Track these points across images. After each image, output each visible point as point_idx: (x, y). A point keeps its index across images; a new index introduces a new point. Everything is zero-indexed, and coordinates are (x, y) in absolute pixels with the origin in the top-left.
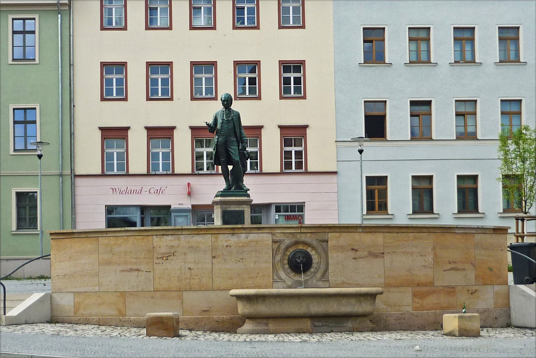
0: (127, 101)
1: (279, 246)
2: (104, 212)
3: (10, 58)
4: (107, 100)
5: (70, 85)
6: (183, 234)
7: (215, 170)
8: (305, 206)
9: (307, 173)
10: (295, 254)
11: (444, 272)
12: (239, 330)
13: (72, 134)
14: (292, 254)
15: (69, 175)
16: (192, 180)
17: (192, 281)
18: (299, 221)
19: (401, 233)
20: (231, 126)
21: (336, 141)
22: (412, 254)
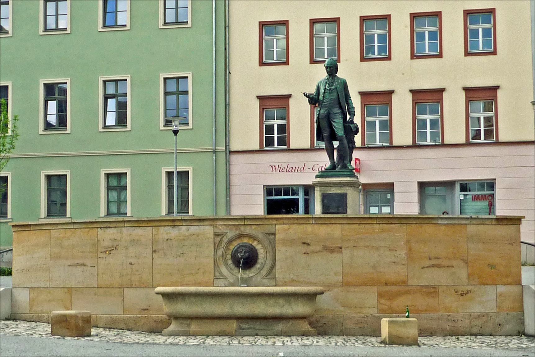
1: (221, 240)
2: (262, 193)
3: (161, 22)
4: (421, 57)
5: (225, 49)
6: (125, 226)
8: (495, 183)
9: (498, 143)
10: (238, 248)
11: (422, 269)
12: (165, 331)
13: (227, 106)
14: (235, 248)
15: (224, 151)
17: (133, 278)
18: (489, 202)
19: (363, 225)
20: (334, 95)
22: (378, 248)
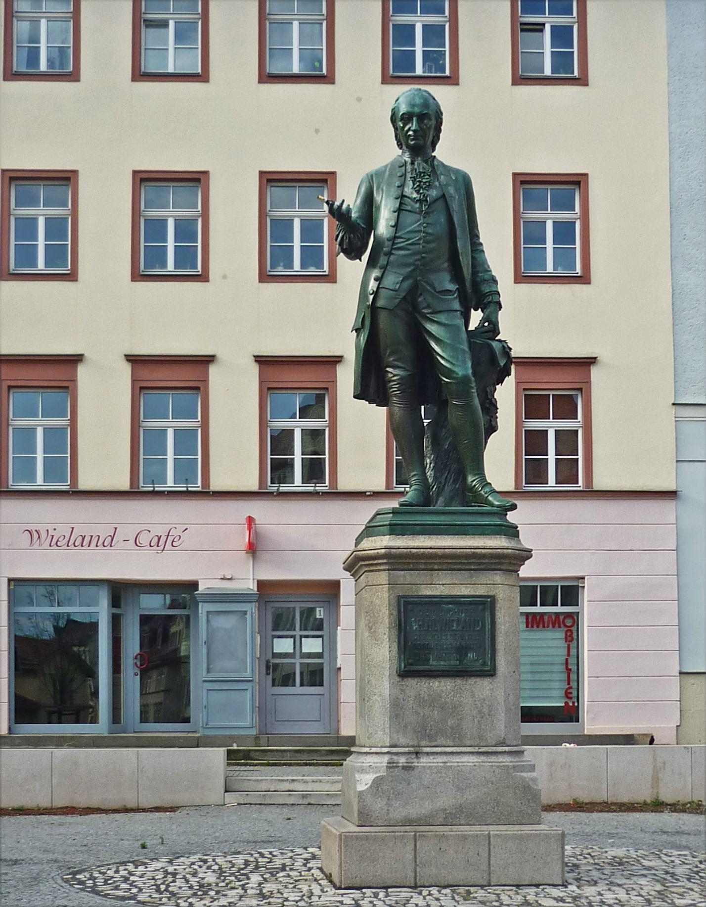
0: (76, 280)
7: (327, 484)
9: (591, 494)
16: (258, 509)
18: (567, 631)
21: (674, 404)
